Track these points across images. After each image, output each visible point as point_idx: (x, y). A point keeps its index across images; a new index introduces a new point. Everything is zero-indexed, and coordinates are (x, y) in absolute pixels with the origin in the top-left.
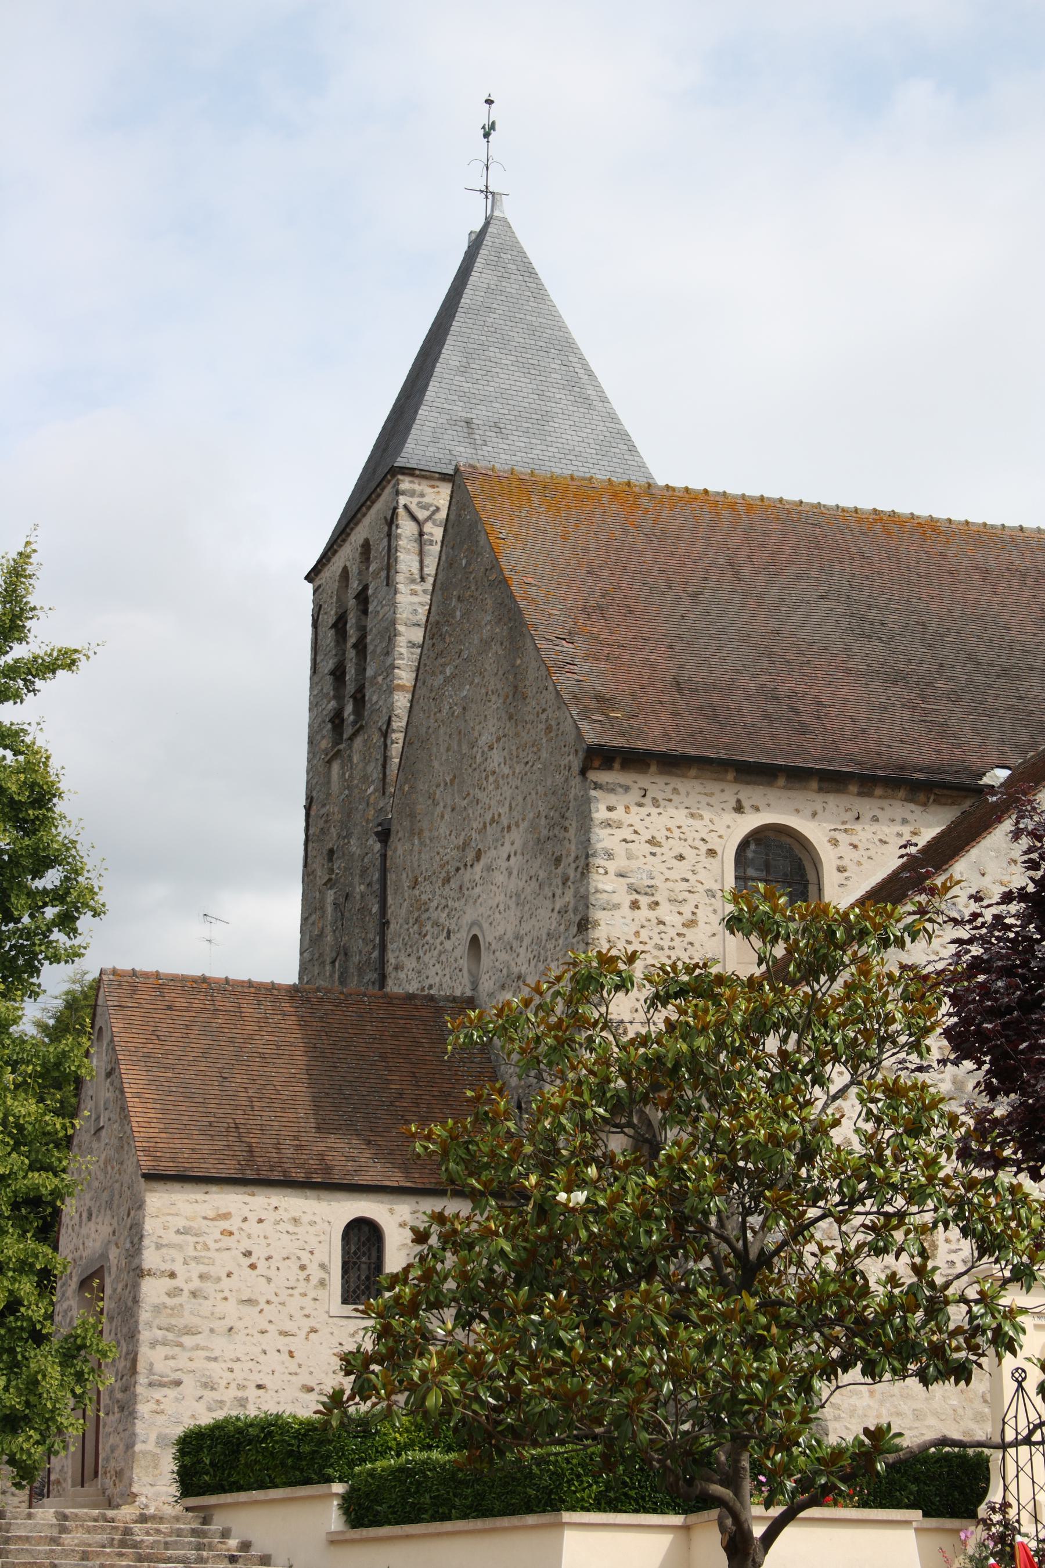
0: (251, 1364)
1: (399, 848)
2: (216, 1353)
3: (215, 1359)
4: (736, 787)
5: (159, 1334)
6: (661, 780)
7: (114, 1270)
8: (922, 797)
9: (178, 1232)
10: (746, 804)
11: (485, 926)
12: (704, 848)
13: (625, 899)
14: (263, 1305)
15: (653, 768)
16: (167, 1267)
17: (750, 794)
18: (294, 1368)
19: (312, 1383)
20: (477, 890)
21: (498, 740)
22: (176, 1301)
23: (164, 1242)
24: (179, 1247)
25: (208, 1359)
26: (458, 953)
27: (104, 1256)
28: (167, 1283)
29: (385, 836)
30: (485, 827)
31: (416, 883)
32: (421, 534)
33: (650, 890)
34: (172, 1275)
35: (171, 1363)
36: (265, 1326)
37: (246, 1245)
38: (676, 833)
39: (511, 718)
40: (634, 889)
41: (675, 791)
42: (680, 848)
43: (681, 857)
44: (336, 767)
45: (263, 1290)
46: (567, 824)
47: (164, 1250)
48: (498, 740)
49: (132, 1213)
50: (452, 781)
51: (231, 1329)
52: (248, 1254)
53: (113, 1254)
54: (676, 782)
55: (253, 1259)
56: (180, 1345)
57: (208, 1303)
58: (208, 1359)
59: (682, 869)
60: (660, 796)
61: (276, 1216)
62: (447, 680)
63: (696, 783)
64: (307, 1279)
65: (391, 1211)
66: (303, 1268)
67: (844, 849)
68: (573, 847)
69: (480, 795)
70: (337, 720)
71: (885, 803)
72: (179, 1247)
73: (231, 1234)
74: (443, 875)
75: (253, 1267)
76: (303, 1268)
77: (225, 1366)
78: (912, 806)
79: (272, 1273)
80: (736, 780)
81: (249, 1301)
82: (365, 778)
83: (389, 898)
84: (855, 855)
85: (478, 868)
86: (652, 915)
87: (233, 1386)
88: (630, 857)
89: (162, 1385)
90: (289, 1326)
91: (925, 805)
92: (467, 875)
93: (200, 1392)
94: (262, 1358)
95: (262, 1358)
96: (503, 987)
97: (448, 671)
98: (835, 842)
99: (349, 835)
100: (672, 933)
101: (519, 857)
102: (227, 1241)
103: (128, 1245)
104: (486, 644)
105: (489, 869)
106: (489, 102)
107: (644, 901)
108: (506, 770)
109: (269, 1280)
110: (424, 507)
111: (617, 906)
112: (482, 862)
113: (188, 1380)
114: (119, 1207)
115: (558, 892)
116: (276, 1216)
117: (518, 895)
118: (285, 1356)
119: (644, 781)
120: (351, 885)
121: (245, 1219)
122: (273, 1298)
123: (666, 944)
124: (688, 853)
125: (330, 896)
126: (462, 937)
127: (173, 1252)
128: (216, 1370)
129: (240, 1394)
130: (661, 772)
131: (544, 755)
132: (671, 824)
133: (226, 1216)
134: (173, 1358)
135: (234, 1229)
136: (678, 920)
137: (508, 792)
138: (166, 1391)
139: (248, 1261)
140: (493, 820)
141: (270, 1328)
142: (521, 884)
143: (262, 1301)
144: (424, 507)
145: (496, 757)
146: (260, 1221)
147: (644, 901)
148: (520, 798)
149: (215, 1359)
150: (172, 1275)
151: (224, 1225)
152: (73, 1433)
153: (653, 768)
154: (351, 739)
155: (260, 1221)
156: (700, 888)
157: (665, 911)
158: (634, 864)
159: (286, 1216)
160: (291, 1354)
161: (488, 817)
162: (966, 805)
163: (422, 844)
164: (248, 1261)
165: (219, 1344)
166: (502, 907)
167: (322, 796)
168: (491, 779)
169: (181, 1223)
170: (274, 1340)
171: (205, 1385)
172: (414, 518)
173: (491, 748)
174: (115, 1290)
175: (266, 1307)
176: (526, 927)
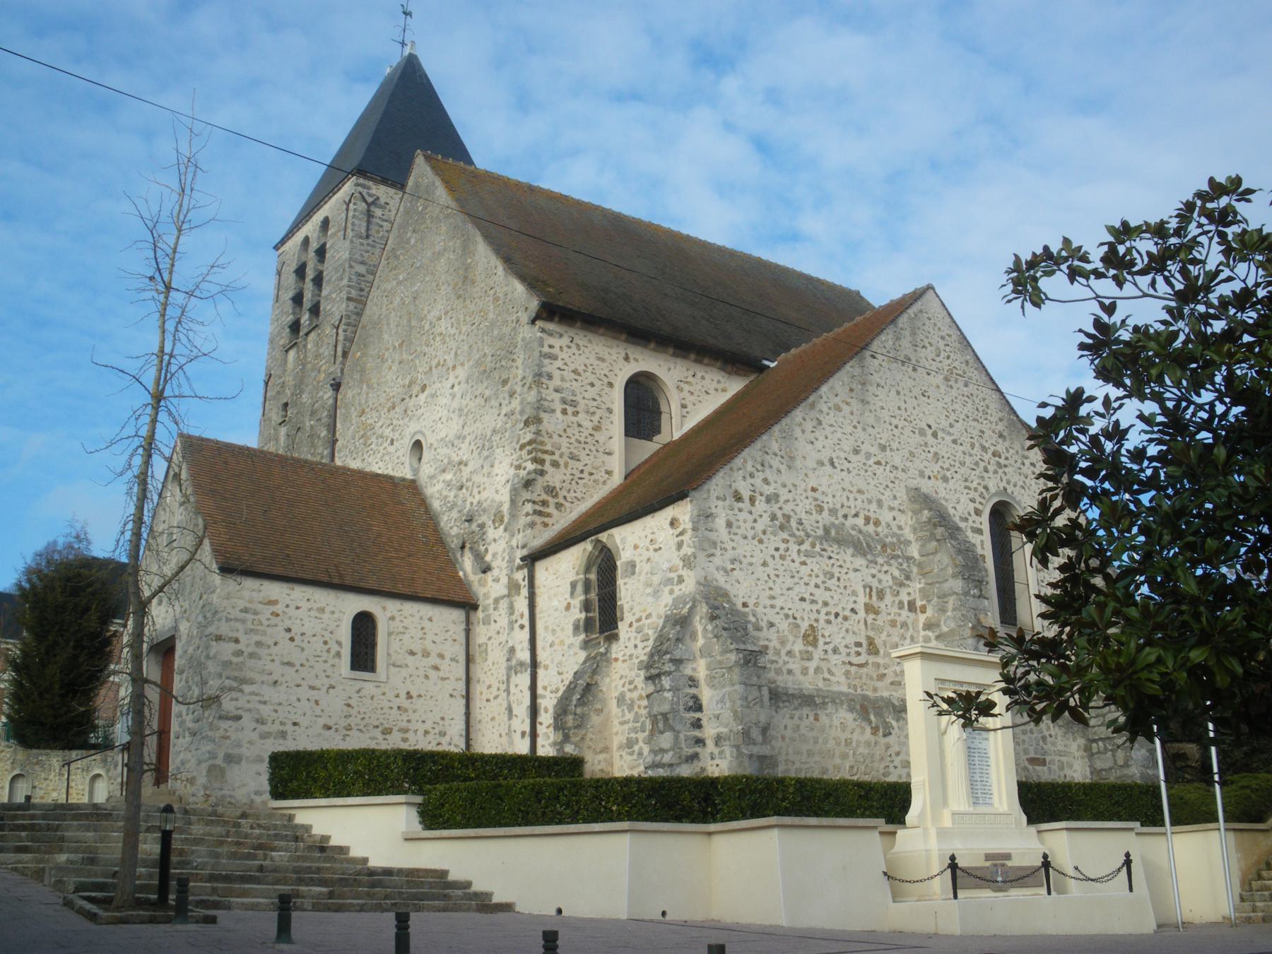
0: (290, 708)
1: (347, 393)
2: (266, 698)
3: (265, 703)
4: (626, 345)
5: (228, 683)
6: (582, 333)
7: (184, 638)
8: (729, 368)
9: (241, 611)
10: (631, 356)
11: (428, 433)
12: (606, 380)
13: (558, 407)
14: (298, 667)
15: (578, 324)
16: (234, 635)
17: (634, 351)
18: (318, 712)
19: (330, 724)
20: (420, 411)
21: (446, 313)
22: (240, 659)
23: (232, 617)
24: (243, 621)
25: (260, 702)
26: (400, 453)
27: (176, 628)
28: (232, 646)
29: (337, 386)
30: (431, 369)
31: (363, 412)
32: (369, 211)
33: (574, 404)
34: (237, 641)
35: (234, 703)
36: (299, 681)
37: (288, 624)
38: (590, 369)
39: (459, 297)
40: (564, 401)
41: (590, 341)
42: (592, 378)
43: (592, 385)
44: (292, 353)
45: (297, 657)
46: (515, 357)
47: (232, 623)
48: (446, 313)
49: (205, 597)
50: (401, 345)
51: (276, 682)
52: (289, 630)
53: (184, 627)
54: (590, 336)
55: (292, 634)
56: (241, 691)
57: (261, 663)
58: (260, 702)
59: (592, 392)
60: (581, 343)
61: (309, 605)
62: (399, 283)
63: (602, 338)
64: (328, 651)
65: (384, 608)
66: (325, 643)
67: (685, 394)
68: (520, 372)
69: (425, 349)
70: (295, 327)
71: (708, 369)
72: (243, 621)
73: (277, 615)
74: (389, 404)
75: (292, 639)
76: (325, 643)
77: (272, 708)
78: (723, 373)
79: (305, 645)
80: (626, 341)
81: (289, 664)
82: (317, 356)
83: (338, 425)
84: (692, 398)
85: (422, 397)
86: (574, 419)
87: (277, 722)
88: (563, 379)
89: (227, 718)
90: (317, 683)
91: (730, 373)
92: (411, 403)
93: (254, 725)
94: (297, 704)
95: (297, 704)
96: (444, 471)
97: (401, 277)
98: (680, 389)
99: (302, 392)
100: (586, 433)
101: (463, 386)
102: (274, 620)
103: (200, 619)
104: (439, 255)
105: (433, 396)
107: (570, 410)
108: (453, 331)
109: (303, 649)
110: (370, 195)
111: (553, 411)
112: (426, 393)
113: (246, 717)
114: (190, 593)
115: (504, 403)
116: (309, 605)
117: (460, 410)
118: (313, 704)
119: (572, 332)
120: (303, 422)
121: (287, 606)
122: (305, 662)
123: (582, 439)
124: (596, 382)
125: (283, 431)
126: (407, 443)
127: (238, 625)
128: (265, 711)
129: (282, 728)
130: (583, 328)
131: (491, 316)
132: (587, 362)
133: (274, 603)
134: (237, 699)
135: (280, 612)
136: (590, 425)
137: (453, 344)
138: (230, 723)
139: (288, 635)
140: (438, 364)
141: (303, 683)
142: (464, 402)
143: (298, 664)
144: (370, 195)
145: (443, 326)
146: (298, 608)
147: (570, 410)
148: (466, 348)
149: (265, 703)
150: (237, 641)
151: (272, 608)
152: (1119, 773)
153: (578, 324)
154: (307, 334)
155: (298, 608)
156: (603, 406)
157: (582, 417)
158: (567, 385)
159: (315, 606)
160: (317, 703)
161: (434, 363)
162: (753, 377)
163: (370, 387)
164: (288, 635)
165: (268, 692)
166: (444, 420)
167: (279, 372)
168: (438, 339)
169: (241, 604)
170: (304, 692)
171: (257, 721)
172: (365, 201)
173: (439, 319)
174: (185, 652)
175: (301, 669)
176: (467, 430)
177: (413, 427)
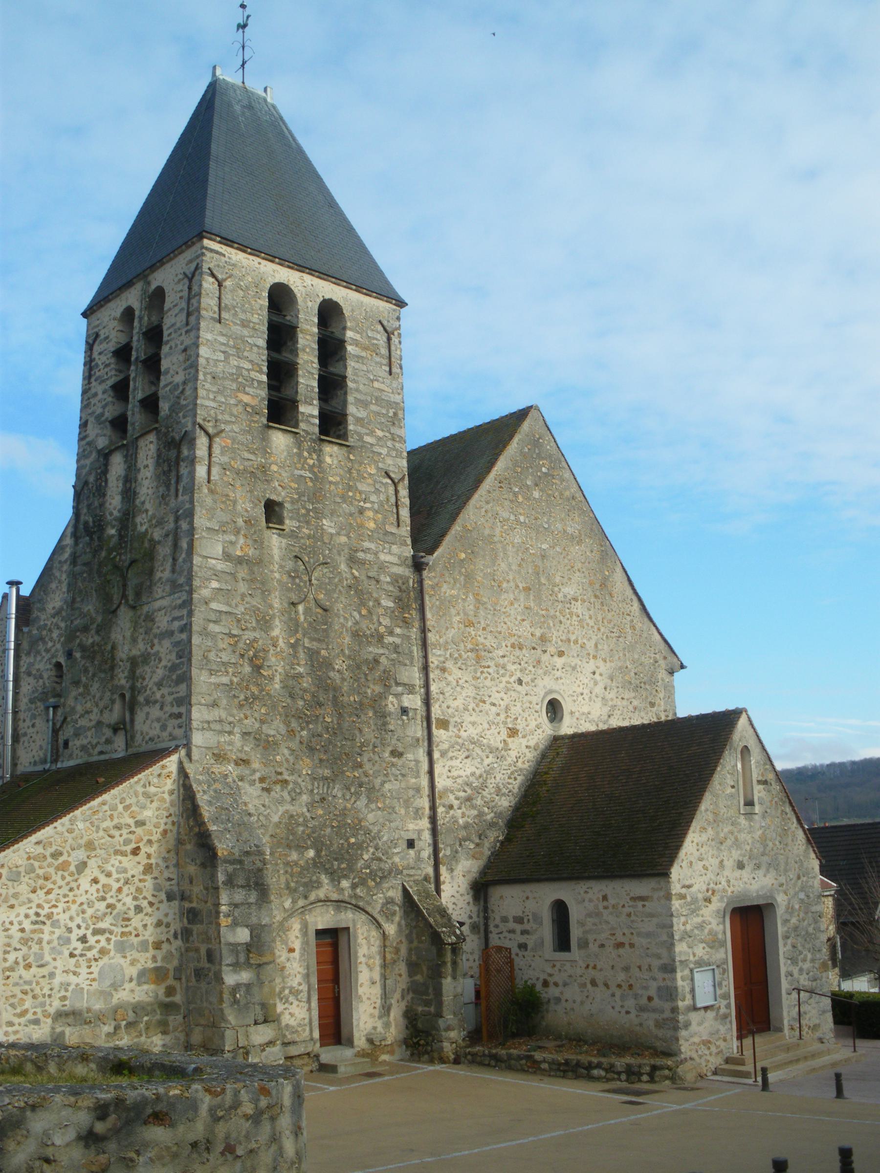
85: (559, 662)
106: (243, 6)
177: (547, 683)
